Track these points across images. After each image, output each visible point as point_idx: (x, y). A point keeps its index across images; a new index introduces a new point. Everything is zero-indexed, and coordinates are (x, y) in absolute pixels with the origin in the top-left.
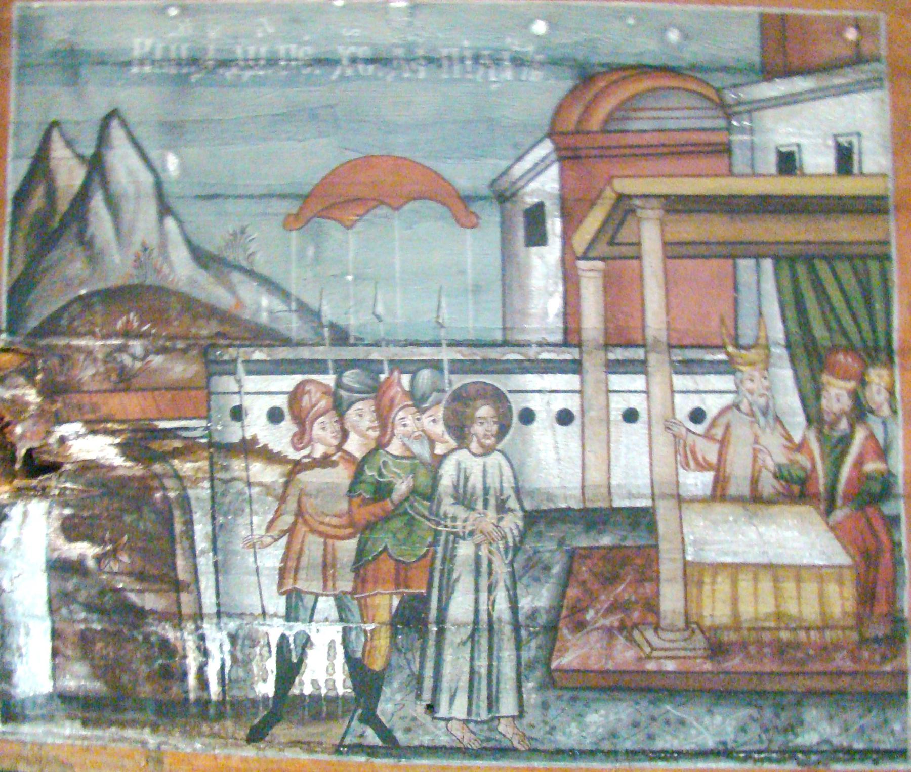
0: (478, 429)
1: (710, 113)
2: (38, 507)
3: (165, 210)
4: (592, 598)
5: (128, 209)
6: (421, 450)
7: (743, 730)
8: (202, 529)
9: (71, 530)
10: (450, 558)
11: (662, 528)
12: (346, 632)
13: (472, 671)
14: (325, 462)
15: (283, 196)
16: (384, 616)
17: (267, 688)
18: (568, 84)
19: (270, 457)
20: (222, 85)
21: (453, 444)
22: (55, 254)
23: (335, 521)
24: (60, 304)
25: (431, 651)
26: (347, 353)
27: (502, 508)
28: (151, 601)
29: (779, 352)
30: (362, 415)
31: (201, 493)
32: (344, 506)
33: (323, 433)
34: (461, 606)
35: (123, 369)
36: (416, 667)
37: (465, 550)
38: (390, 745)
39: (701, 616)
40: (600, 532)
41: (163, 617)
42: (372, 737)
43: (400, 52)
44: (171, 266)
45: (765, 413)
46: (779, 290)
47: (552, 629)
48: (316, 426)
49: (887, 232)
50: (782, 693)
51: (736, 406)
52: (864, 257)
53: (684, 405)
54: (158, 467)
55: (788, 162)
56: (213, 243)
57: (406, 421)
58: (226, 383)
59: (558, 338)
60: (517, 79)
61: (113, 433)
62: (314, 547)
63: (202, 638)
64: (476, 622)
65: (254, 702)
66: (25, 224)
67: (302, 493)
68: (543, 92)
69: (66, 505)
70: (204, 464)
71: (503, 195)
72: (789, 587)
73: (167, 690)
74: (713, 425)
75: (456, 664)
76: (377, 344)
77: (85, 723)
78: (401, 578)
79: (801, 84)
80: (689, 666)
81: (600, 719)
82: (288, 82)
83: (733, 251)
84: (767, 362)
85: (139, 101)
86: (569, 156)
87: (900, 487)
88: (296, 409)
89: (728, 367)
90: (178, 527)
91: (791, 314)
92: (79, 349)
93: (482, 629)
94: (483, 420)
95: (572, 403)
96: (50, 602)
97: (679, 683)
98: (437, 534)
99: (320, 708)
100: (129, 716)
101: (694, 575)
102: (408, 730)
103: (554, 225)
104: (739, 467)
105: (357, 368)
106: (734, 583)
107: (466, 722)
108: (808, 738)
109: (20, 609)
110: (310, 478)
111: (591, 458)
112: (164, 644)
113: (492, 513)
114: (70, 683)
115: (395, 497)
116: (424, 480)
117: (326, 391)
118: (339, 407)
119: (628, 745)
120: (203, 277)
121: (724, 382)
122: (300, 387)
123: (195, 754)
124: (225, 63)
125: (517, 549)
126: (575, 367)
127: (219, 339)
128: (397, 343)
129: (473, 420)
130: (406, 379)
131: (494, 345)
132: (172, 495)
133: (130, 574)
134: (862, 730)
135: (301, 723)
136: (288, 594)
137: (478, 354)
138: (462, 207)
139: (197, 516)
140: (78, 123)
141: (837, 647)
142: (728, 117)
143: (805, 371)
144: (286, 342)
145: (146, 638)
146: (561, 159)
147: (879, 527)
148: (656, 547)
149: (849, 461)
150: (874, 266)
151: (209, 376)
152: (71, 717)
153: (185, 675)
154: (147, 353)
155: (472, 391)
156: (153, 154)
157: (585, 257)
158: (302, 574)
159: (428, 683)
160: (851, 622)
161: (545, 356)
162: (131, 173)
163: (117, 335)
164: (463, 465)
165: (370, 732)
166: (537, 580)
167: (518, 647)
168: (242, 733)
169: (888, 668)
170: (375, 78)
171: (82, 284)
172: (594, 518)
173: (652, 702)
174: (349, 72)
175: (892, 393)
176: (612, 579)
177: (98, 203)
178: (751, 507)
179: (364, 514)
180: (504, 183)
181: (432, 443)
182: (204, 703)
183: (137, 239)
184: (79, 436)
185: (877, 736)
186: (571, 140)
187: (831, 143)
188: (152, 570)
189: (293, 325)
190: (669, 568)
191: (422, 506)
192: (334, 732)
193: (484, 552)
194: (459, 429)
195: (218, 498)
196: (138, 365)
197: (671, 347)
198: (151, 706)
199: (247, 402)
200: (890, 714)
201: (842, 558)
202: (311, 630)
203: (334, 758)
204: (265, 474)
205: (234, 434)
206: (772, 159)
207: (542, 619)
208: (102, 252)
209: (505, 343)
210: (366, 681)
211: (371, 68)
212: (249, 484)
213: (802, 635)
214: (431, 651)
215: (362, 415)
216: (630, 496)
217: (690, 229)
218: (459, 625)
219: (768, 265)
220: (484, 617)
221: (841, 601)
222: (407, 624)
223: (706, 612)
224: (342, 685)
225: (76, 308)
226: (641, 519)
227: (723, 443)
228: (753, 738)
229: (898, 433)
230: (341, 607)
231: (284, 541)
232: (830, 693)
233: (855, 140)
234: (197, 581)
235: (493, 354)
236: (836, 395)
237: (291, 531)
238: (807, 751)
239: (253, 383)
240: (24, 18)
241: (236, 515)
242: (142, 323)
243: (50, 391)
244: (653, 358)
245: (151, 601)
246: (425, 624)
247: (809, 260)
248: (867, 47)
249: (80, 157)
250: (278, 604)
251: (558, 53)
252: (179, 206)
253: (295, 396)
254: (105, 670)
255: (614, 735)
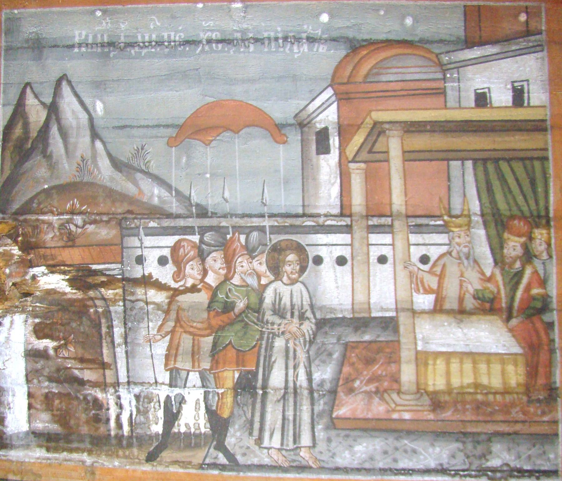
0: (288, 268)
1: (433, 69)
2: (19, 318)
3: (95, 135)
4: (359, 373)
5: (73, 133)
6: (252, 281)
7: (453, 456)
8: (118, 331)
9: (40, 332)
10: (270, 347)
11: (402, 329)
12: (206, 394)
13: (284, 419)
14: (194, 289)
15: (167, 126)
16: (229, 384)
17: (158, 428)
18: (343, 53)
19: (160, 286)
20: (130, 57)
21: (272, 278)
22: (28, 165)
23: (199, 325)
24: (29, 196)
25: (258, 406)
26: (206, 222)
27: (302, 317)
28: (88, 375)
29: (477, 219)
30: (216, 261)
31: (117, 309)
32: (205, 315)
33: (192, 271)
34: (277, 378)
35: (70, 233)
36: (249, 415)
37: (279, 343)
38: (233, 464)
39: (426, 384)
40: (364, 332)
41: (95, 385)
42: (222, 459)
43: (238, 35)
44: (98, 169)
45: (467, 258)
46: (476, 181)
47: (333, 392)
48: (188, 267)
49: (546, 143)
50: (479, 434)
51: (450, 253)
52: (531, 159)
53: (416, 253)
54: (91, 293)
55: (482, 100)
56: (125, 152)
57: (242, 264)
58: (134, 241)
59: (337, 211)
60: (310, 49)
61: (64, 273)
62: (186, 341)
63: (119, 397)
64: (286, 388)
65: (151, 437)
66: (10, 145)
67: (179, 309)
68: (327, 57)
69: (36, 317)
70: (120, 291)
71: (302, 124)
72: (483, 367)
73: (97, 429)
74: (434, 265)
75: (273, 414)
76: (225, 216)
77: (48, 450)
78: (240, 361)
79: (490, 50)
80: (420, 416)
81: (363, 449)
82: (167, 56)
83: (447, 156)
84: (469, 225)
85: (78, 68)
86: (343, 98)
87: (554, 305)
88: (176, 257)
89: (445, 229)
90: (104, 330)
91: (484, 196)
92: (44, 222)
93: (291, 392)
94: (290, 263)
95: (346, 252)
96: (27, 376)
97: (412, 427)
98: (262, 333)
99: (191, 441)
100: (75, 445)
101: (423, 359)
102: (244, 455)
103: (334, 141)
104: (451, 290)
105: (211, 231)
106: (448, 363)
107: (279, 450)
108: (495, 462)
109: (9, 380)
110: (185, 299)
111: (358, 286)
112: (96, 400)
113: (296, 320)
114: (39, 426)
115: (237, 310)
116: (254, 299)
117: (194, 245)
118: (202, 256)
119: (381, 465)
120: (118, 176)
121: (442, 238)
122: (178, 242)
123: (114, 469)
124: (131, 45)
125: (311, 342)
126: (348, 229)
127: (132, 216)
128: (236, 216)
129: (284, 262)
130: (243, 238)
131: (297, 216)
132: (100, 310)
133: (74, 359)
134: (529, 457)
135: (179, 449)
136: (171, 370)
137: (289, 222)
138: (277, 131)
139: (115, 323)
140: (42, 83)
141: (513, 404)
142: (444, 72)
143: (493, 232)
144: (169, 216)
145: (85, 398)
146: (339, 100)
147: (539, 325)
148: (398, 341)
149: (522, 287)
150: (537, 164)
151: (123, 237)
152: (40, 446)
153: (108, 420)
154: (85, 223)
155: (283, 245)
156: (87, 101)
157: (353, 161)
158: (179, 358)
159: (257, 426)
160: (521, 389)
161: (329, 223)
162: (73, 112)
163: (67, 213)
164: (279, 291)
165: (221, 455)
166: (324, 362)
167: (312, 404)
168: (143, 456)
169: (545, 419)
170: (222, 51)
171: (45, 181)
172: (360, 322)
173: (397, 439)
174: (207, 48)
175: (549, 245)
176: (369, 362)
177: (54, 130)
178: (459, 316)
179: (216, 322)
180: (304, 115)
181: (259, 277)
182: (119, 438)
183: (78, 154)
184: (44, 274)
185: (539, 462)
186: (343, 88)
187: (509, 86)
188: (88, 356)
189: (175, 207)
190: (406, 354)
191: (253, 316)
192: (198, 456)
193: (291, 345)
194: (276, 269)
195: (128, 312)
196: (79, 230)
197: (408, 216)
198: (88, 440)
199: (146, 253)
200: (547, 447)
201: (517, 349)
202: (184, 392)
203: (200, 471)
204: (159, 297)
205: (138, 272)
206: (472, 97)
207: (328, 386)
208: (57, 163)
209: (304, 215)
210: (219, 424)
211: (220, 46)
212: (147, 303)
213: (491, 397)
214: (258, 406)
215: (216, 261)
216: (382, 309)
217: (420, 142)
218: (276, 390)
219: (469, 164)
220: (291, 384)
221: (516, 376)
222: (244, 389)
223: (430, 382)
224: (204, 427)
225: (42, 197)
226: (389, 324)
227: (441, 277)
228: (459, 462)
229: (553, 270)
230: (203, 378)
231: (168, 338)
232: (509, 434)
233: (525, 84)
234: (116, 362)
235: (298, 222)
236: (513, 246)
237: (173, 332)
238: (494, 470)
239: (149, 241)
240: (8, 19)
241: (139, 322)
242: (82, 205)
243: (26, 247)
244: (397, 224)
245: (88, 375)
246: (255, 388)
247: (496, 161)
248: (533, 25)
249: (43, 104)
250: (164, 377)
251: (335, 34)
252: (104, 134)
253: (175, 249)
254: (62, 418)
255: (372, 459)
